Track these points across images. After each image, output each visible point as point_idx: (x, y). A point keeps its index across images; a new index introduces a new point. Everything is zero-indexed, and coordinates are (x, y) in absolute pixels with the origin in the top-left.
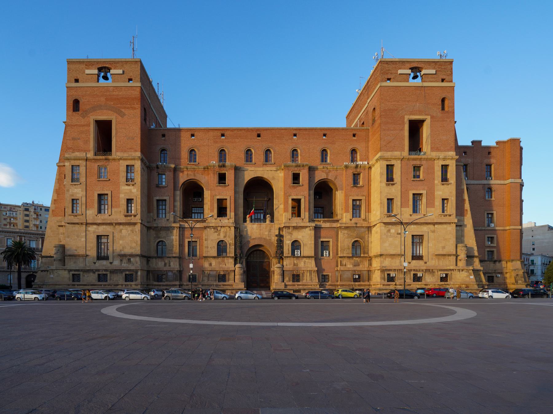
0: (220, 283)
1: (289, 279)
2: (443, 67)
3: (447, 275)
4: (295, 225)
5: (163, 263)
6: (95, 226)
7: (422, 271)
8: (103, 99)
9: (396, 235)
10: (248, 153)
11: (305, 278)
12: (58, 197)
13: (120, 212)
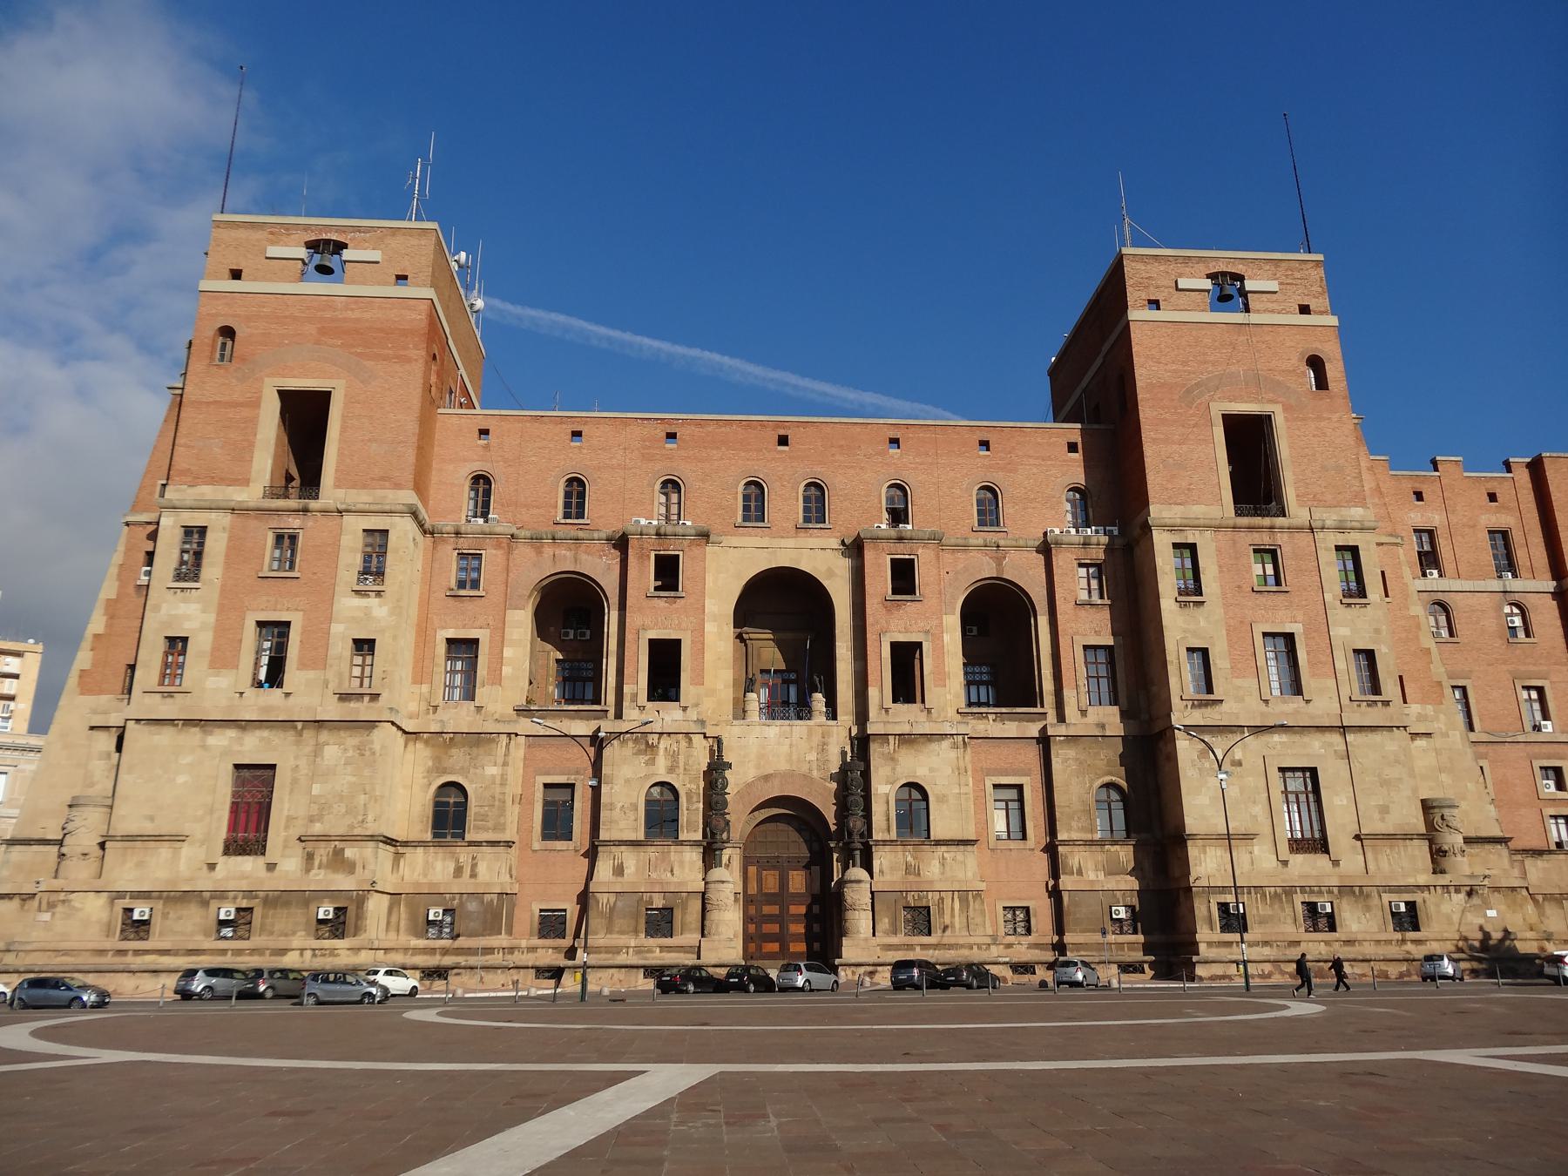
2: (1298, 275)
3: (1411, 905)
4: (906, 729)
5: (451, 866)
6: (232, 733)
7: (1330, 892)
8: (311, 329)
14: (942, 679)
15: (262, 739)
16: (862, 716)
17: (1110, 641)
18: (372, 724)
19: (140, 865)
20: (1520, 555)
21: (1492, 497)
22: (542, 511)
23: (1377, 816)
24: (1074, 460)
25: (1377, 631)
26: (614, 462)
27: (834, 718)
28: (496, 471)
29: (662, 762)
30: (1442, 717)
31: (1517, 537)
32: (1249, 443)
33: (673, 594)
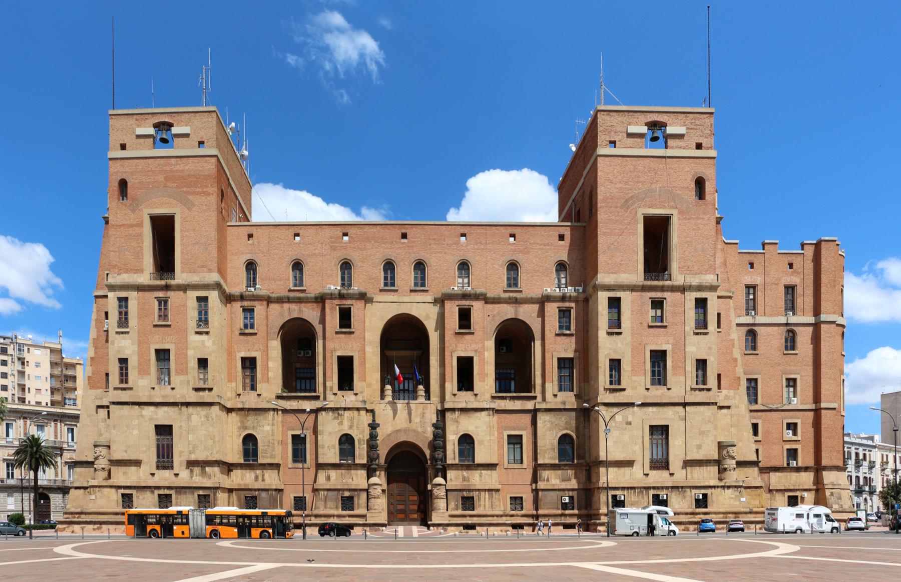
0: (345, 513)
1: (457, 505)
2: (698, 122)
3: (705, 496)
6: (152, 408)
8: (161, 178)
9: (624, 426)
10: (389, 266)
11: (482, 502)
12: (95, 353)
13: (188, 382)
14: (484, 376)
15: (165, 412)
16: (443, 399)
17: (571, 355)
18: (210, 404)
19: (125, 473)
20: (799, 301)
21: (791, 266)
22: (281, 283)
23: (695, 450)
24: (562, 246)
25: (710, 348)
26: (317, 251)
27: (429, 399)
28: (259, 259)
29: (346, 424)
30: (737, 397)
31: (799, 291)
32: (657, 233)
33: (347, 330)
